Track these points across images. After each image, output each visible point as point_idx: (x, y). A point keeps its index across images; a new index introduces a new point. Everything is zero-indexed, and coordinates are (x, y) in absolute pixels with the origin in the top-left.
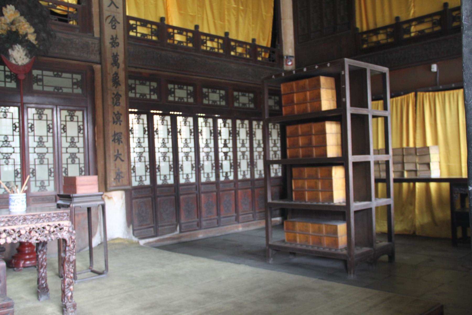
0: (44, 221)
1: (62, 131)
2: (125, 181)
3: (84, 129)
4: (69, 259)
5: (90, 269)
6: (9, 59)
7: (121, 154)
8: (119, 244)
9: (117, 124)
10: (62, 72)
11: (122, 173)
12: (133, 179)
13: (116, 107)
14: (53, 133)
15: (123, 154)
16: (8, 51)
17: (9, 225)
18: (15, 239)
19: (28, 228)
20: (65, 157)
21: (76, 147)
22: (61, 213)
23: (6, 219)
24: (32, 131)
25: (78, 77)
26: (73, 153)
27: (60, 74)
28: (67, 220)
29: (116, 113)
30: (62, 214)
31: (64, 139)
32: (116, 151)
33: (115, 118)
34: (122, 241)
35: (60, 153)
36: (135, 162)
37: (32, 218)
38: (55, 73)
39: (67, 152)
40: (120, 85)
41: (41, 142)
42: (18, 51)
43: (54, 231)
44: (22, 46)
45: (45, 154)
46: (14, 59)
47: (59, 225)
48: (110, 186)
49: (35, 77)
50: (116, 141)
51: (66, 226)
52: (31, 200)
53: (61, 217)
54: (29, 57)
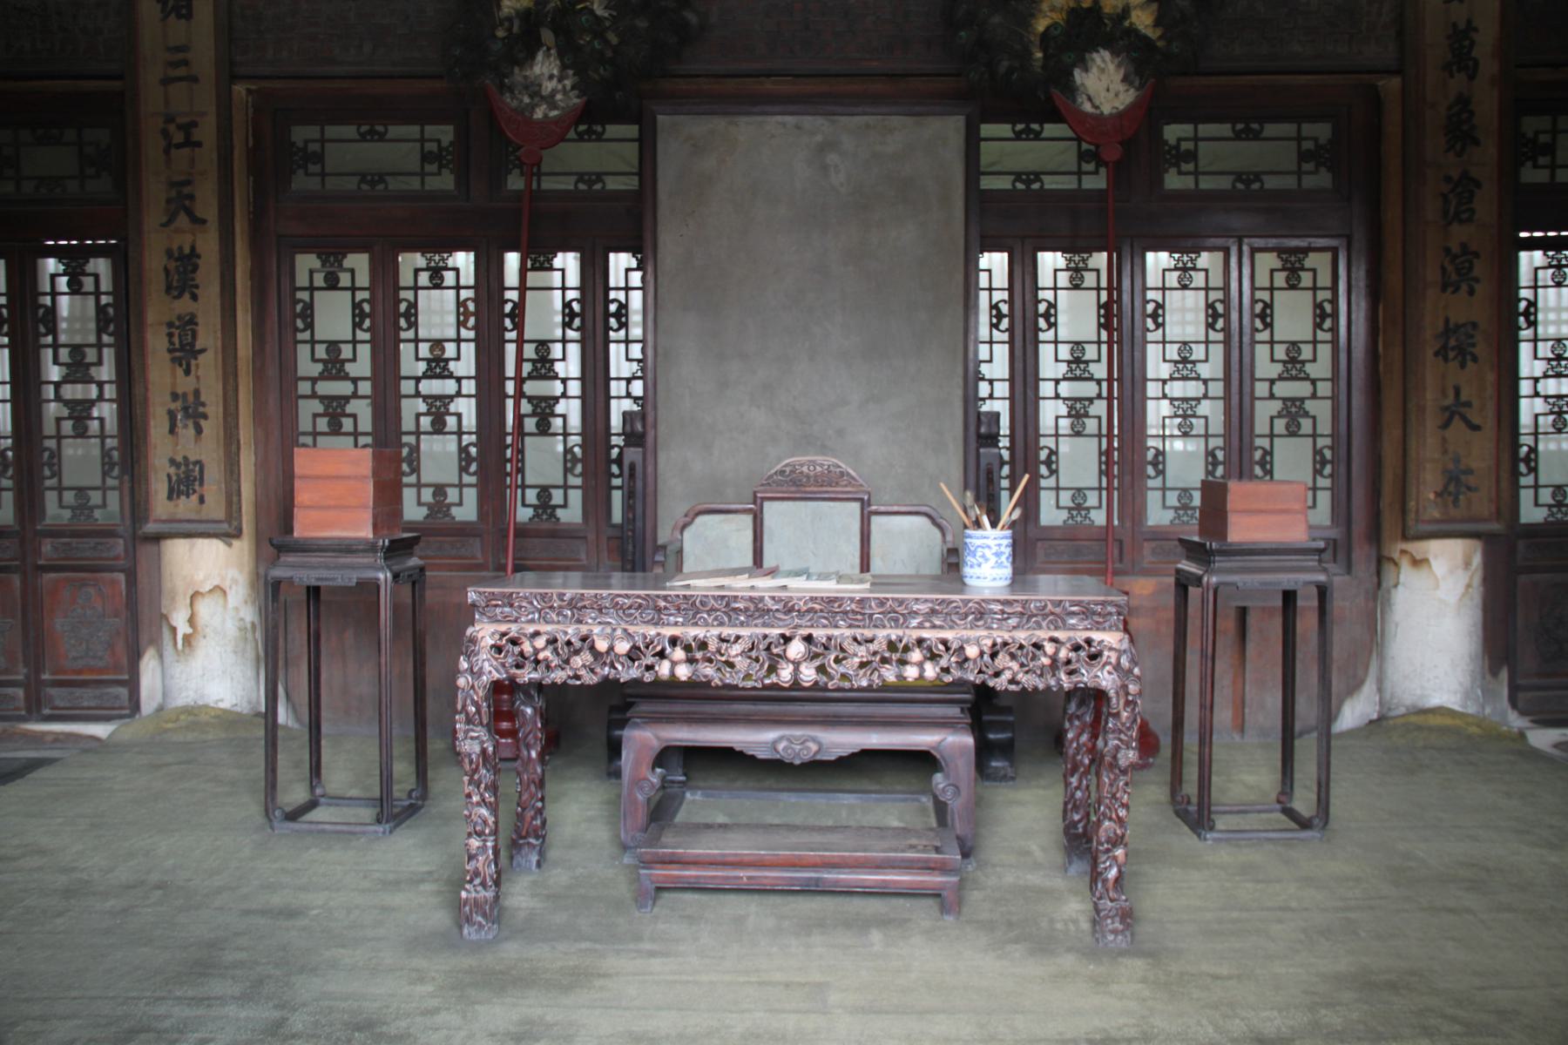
0: (1040, 627)
1: (1258, 324)
2: (1481, 502)
3: (1335, 315)
4: (1115, 757)
5: (1279, 802)
6: (1074, 101)
7: (1468, 404)
8: (1443, 730)
9: (1457, 290)
10: (1264, 119)
11: (1469, 471)
12: (1526, 496)
13: (1455, 227)
14: (1226, 330)
15: (1476, 403)
16: (1072, 75)
17: (934, 627)
18: (946, 670)
19: (989, 642)
20: (1264, 411)
21: (1307, 378)
22: (1096, 604)
23: (924, 608)
24: (1158, 326)
25: (1321, 131)
26: (1293, 400)
27: (1255, 126)
28: (1118, 630)
29: (1455, 249)
30: (1099, 608)
31: (1262, 352)
32: (1451, 394)
33: (1450, 268)
34: (1458, 722)
35: (1247, 399)
36: (1536, 434)
37: (1003, 612)
38: (1240, 126)
39: (1272, 396)
40: (1477, 143)
41: (1184, 361)
42: (1102, 70)
43: (1069, 662)
44: (1115, 53)
45: (451, 398)
46: (1090, 99)
47: (1089, 642)
48: (1417, 521)
49: (1172, 148)
50: (1451, 354)
51: (1111, 649)
52: (1028, 550)
53: (1096, 618)
54: (1137, 83)
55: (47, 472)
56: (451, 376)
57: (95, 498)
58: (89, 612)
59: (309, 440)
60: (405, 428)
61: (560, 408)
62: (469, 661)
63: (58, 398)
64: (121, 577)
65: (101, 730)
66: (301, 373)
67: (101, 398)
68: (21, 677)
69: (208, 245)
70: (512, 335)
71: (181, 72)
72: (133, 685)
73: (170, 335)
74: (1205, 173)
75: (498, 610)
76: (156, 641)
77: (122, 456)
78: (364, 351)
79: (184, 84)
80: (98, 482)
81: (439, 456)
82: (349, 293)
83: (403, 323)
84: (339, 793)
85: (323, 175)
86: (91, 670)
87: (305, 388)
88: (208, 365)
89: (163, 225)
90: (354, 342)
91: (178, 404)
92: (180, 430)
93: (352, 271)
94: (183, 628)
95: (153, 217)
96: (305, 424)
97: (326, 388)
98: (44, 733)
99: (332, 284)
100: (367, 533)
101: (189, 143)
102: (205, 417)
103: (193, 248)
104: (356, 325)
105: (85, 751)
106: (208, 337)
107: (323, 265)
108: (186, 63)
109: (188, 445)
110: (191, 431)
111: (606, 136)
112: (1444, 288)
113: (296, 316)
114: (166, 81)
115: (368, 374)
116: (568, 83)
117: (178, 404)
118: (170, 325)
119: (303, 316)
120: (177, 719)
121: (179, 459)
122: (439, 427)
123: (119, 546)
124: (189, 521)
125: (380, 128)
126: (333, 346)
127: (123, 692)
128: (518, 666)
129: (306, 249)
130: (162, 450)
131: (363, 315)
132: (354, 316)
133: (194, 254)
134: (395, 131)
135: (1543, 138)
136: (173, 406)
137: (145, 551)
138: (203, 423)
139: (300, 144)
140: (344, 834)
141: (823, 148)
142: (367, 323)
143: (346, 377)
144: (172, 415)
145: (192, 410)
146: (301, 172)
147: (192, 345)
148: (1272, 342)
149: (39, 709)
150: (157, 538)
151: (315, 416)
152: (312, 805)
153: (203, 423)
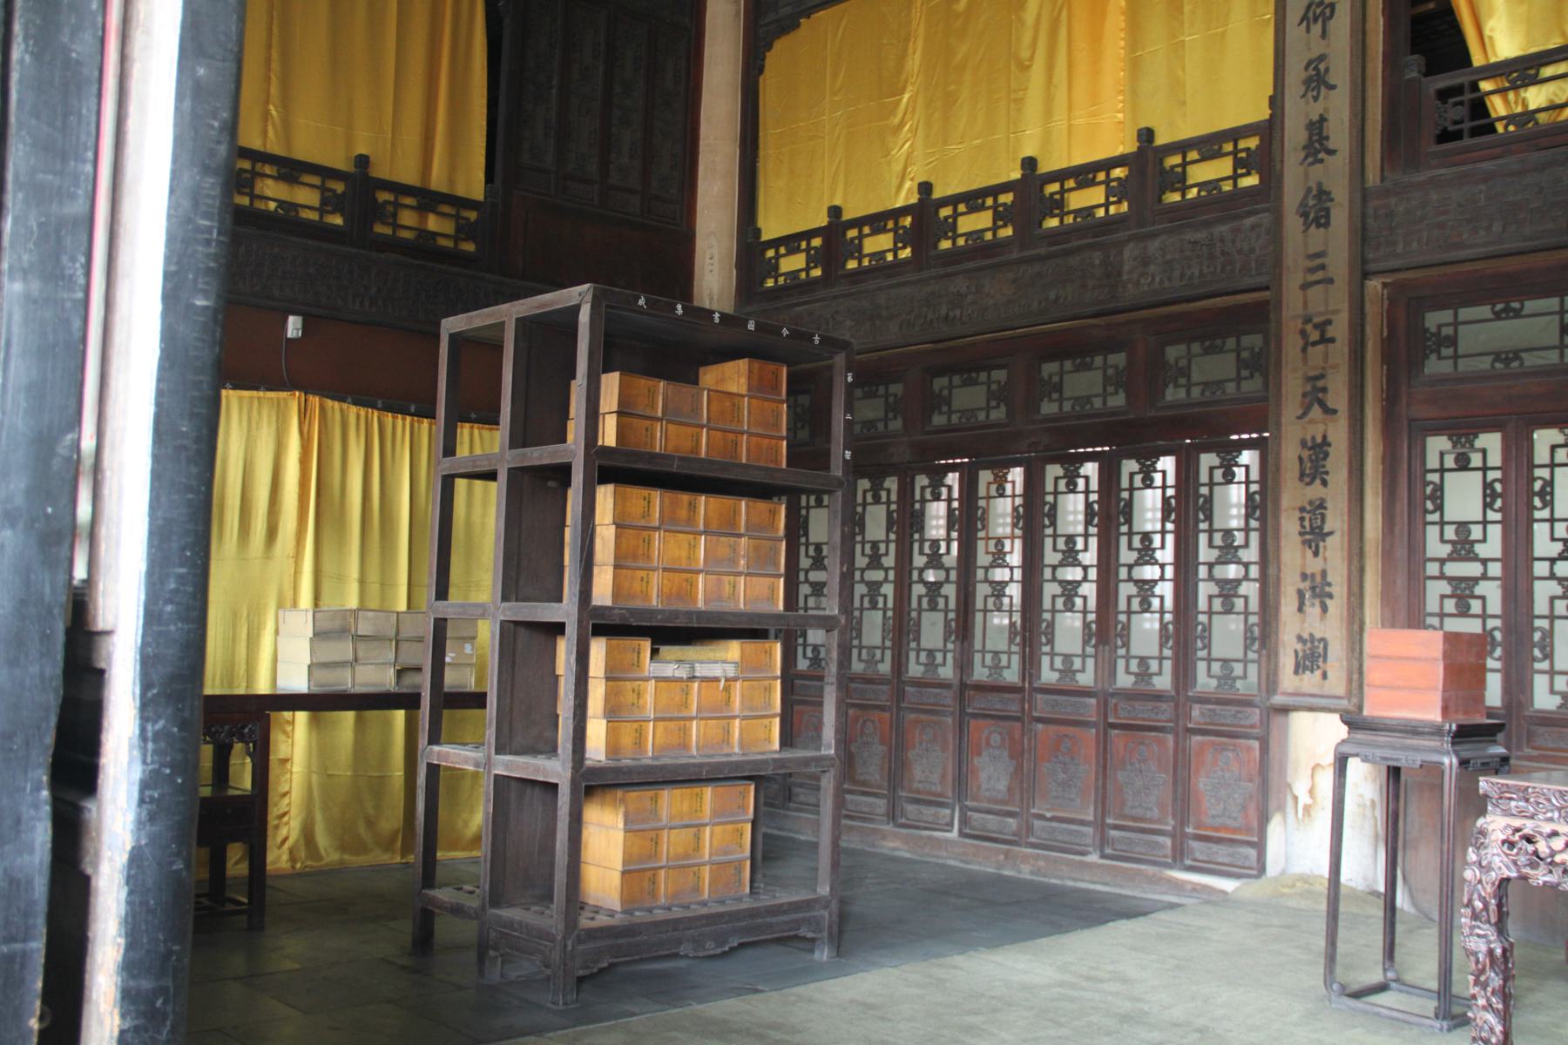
55: (1199, 644)
56: (1156, 563)
57: (1238, 669)
58: (1227, 775)
59: (1435, 621)
60: (1537, 612)
61: (1157, 590)
62: (1478, 855)
63: (1211, 577)
64: (1256, 744)
65: (1228, 885)
66: (1429, 554)
67: (1085, 579)
68: (1169, 828)
71: (1319, 275)
72: (1260, 846)
73: (1302, 519)
74: (1554, 348)
75: (1513, 804)
76: (1281, 808)
77: (1177, 630)
78: (1495, 532)
79: (1320, 287)
80: (1240, 655)
81: (1147, 628)
82: (1480, 474)
83: (1537, 502)
84: (1419, 983)
85: (1456, 357)
86: (1227, 829)
87: (1432, 569)
88: (1335, 548)
89: (1299, 418)
90: (1485, 523)
91: (1307, 584)
92: (1307, 608)
93: (1484, 451)
94: (1304, 799)
95: (1290, 409)
96: (1432, 605)
97: (1453, 569)
98: (1185, 882)
99: (1463, 465)
100: (1435, 716)
101: (1325, 340)
102: (1330, 596)
103: (1325, 437)
104: (1487, 506)
105: (1208, 902)
106: (1336, 520)
107: (1454, 447)
108: (1323, 267)
109: (1314, 623)
110: (1317, 609)
111: (1525, 312)
113: (1426, 498)
114: (1305, 286)
115: (1498, 555)
117: (1307, 584)
118: (1302, 509)
119: (1432, 497)
120: (1293, 886)
121: (1306, 636)
122: (1069, 607)
123: (1255, 716)
124: (1312, 695)
125: (1516, 305)
126: (1463, 526)
127: (1252, 853)
128: (1534, 866)
129: (1437, 431)
130: (1291, 626)
131: (1494, 495)
132: (1485, 496)
134: (1531, 306)
136: (1302, 586)
137: (1277, 720)
138: (1328, 602)
139: (1433, 329)
140: (1399, 1021)
142: (1498, 503)
143: (1476, 558)
144: (1301, 594)
146: (1433, 357)
147: (1321, 528)
149: (1182, 860)
150: (1285, 710)
151: (1443, 597)
152: (1382, 988)
153: (1328, 602)
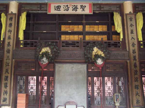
7: (138, 93)
9: (136, 82)
11: (139, 101)
13: (136, 75)
29: (136, 78)
32: (136, 92)
40: (137, 67)
44: (100, 59)
69: (9, 75)
70: (18, 84)
71: (8, 58)
88: (8, 88)
92: (5, 95)
99: (21, 79)
101: (8, 65)
102: (7, 93)
106: (8, 85)
108: (9, 58)
110: (6, 95)
112: (135, 81)
114: (6, 59)
116: (47, 60)
117: (5, 92)
121: (4, 98)
133: (8, 76)
135: (143, 66)
141: (72, 68)
142: (46, 84)
144: (4, 93)
145: (6, 92)
148: (24, 80)
